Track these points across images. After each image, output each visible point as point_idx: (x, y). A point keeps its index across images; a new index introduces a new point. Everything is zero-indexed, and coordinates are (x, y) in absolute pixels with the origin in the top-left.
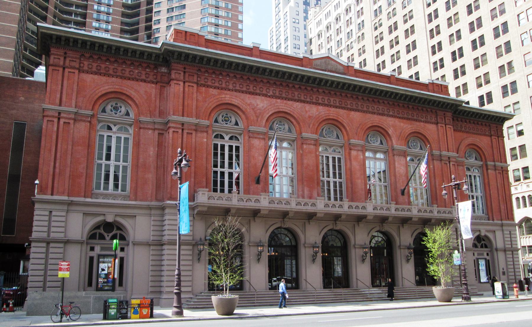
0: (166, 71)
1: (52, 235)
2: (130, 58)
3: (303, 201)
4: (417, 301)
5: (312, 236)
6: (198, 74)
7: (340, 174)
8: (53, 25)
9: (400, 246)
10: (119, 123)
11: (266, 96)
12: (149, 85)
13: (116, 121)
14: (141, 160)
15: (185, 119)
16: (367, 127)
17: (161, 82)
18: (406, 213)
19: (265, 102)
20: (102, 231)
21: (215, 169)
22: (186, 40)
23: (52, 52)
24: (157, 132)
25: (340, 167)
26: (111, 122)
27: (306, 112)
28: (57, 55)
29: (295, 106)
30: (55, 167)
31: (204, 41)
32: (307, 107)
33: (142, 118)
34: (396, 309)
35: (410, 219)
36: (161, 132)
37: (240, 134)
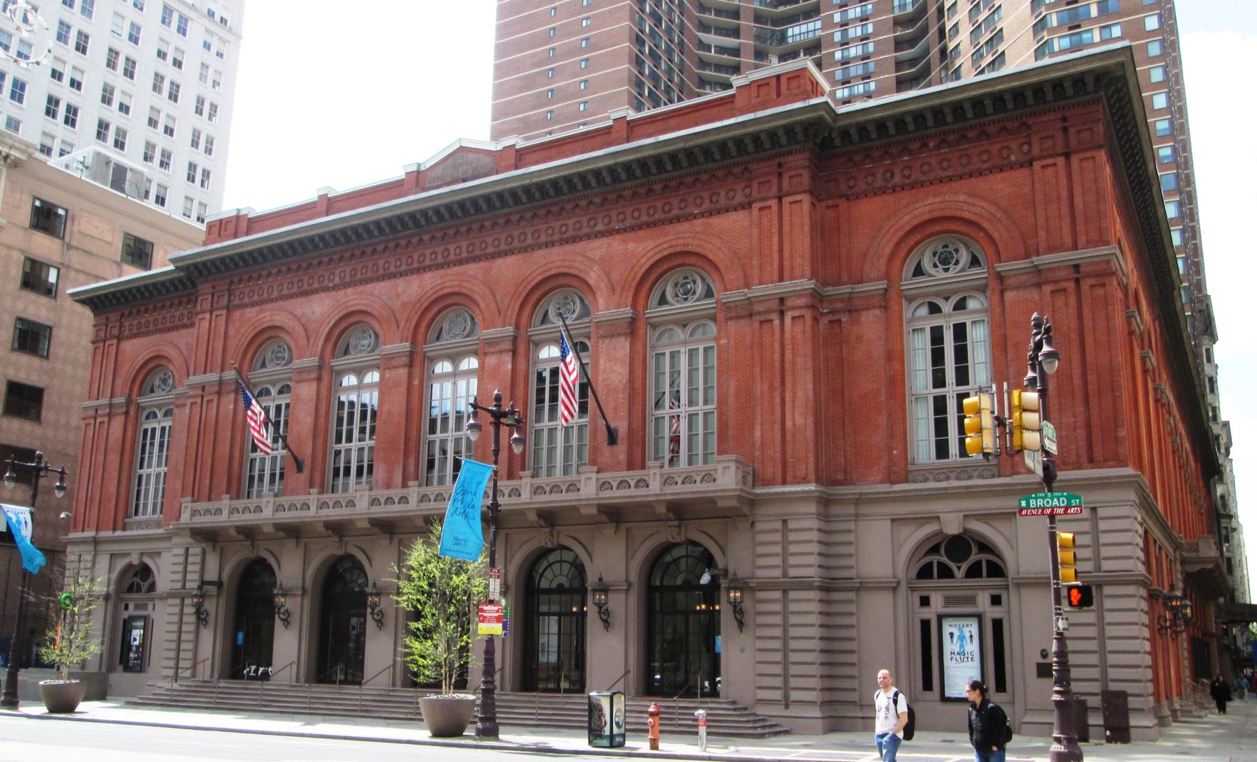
2: (973, 122)
3: (331, 499)
4: (388, 725)
5: (612, 561)
8: (898, 90)
10: (955, 292)
13: (951, 286)
20: (945, 559)
26: (936, 294)
32: (400, 283)
34: (345, 738)
35: (350, 522)
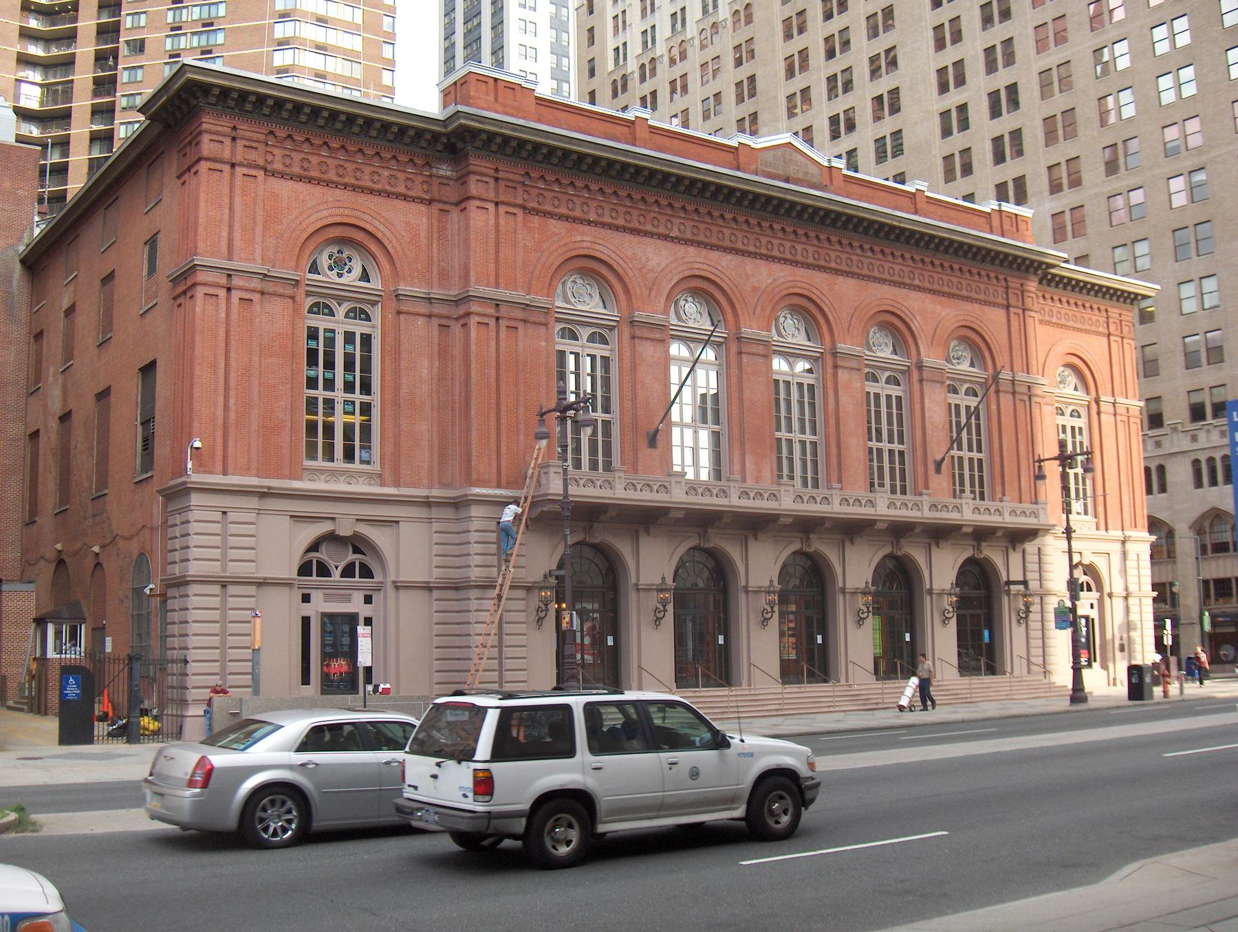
0: (448, 173)
7: (813, 423)
9: (637, 585)
11: (666, 237)
12: (415, 207)
14: (404, 391)
15: (504, 293)
16: (869, 315)
17: (440, 201)
19: (664, 253)
21: (312, 393)
22: (496, 100)
23: (204, 126)
24: (435, 322)
27: (748, 277)
29: (724, 264)
30: (226, 407)
31: (534, 102)
32: (749, 265)
33: (404, 288)
35: (957, 528)
36: (444, 322)
37: (374, 304)
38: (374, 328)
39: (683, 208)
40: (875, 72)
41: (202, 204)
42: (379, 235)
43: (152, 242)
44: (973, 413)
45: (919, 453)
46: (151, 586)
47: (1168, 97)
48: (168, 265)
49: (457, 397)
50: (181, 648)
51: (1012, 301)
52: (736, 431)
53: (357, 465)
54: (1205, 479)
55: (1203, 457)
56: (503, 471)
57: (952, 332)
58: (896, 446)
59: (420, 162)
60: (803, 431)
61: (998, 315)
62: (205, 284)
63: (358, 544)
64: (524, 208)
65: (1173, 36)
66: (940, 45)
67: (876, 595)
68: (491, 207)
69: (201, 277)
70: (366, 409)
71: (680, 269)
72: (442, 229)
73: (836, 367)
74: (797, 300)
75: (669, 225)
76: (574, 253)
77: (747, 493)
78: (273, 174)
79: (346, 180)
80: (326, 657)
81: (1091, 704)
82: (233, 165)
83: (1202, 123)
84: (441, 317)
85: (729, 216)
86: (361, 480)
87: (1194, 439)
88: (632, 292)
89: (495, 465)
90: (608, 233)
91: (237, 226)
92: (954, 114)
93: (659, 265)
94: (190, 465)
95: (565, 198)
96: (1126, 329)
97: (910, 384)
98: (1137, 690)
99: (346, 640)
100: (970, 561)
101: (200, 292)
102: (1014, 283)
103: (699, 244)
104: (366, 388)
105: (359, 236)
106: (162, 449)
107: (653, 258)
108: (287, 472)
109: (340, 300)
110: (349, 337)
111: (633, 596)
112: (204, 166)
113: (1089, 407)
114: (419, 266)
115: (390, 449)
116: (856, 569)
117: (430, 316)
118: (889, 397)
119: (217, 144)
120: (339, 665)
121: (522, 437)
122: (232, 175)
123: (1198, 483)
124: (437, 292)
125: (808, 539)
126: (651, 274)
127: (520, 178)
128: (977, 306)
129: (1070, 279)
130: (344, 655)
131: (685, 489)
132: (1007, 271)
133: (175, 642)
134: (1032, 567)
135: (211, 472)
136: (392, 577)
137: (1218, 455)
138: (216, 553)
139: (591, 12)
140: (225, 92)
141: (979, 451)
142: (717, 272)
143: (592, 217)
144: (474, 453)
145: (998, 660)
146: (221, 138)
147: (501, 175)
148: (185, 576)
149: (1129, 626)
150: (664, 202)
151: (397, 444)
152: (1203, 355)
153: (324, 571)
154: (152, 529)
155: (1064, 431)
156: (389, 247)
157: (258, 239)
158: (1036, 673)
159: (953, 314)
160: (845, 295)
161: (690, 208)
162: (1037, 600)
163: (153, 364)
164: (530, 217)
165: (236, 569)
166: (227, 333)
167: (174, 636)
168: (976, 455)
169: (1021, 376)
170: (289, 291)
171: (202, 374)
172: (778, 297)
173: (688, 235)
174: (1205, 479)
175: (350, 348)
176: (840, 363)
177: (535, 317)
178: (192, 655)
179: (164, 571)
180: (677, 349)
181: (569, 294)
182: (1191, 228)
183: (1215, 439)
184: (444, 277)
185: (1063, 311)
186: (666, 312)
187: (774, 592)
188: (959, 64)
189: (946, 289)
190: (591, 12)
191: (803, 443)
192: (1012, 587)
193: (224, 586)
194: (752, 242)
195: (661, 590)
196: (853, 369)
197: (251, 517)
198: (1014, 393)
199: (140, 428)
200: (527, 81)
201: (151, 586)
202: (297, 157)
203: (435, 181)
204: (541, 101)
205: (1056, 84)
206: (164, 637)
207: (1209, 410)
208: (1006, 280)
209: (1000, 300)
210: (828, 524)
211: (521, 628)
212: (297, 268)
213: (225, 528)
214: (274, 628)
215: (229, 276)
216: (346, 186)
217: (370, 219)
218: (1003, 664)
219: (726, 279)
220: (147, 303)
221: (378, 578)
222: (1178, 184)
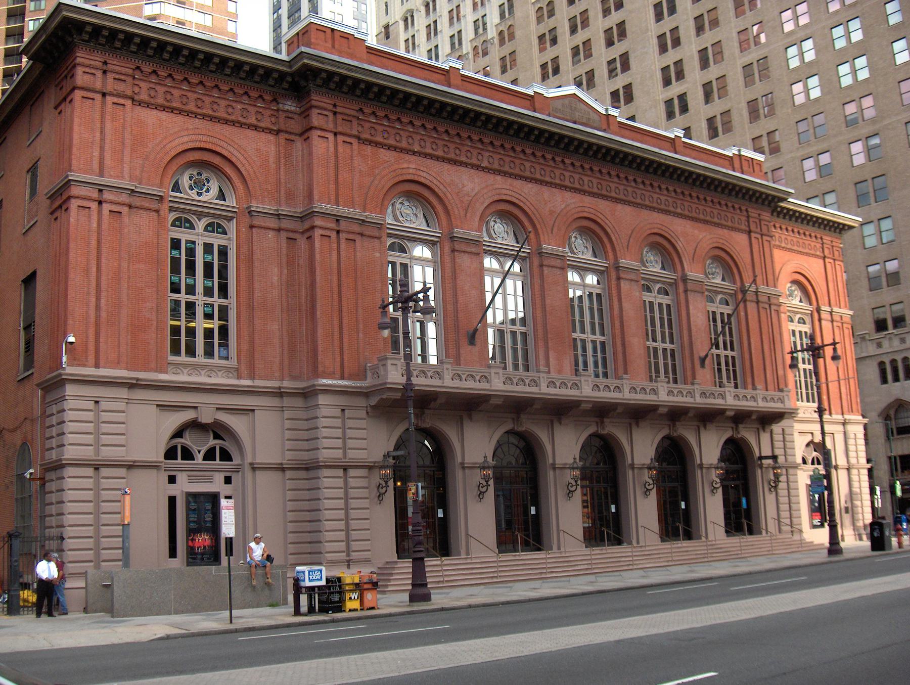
0: (293, 108)
1: (351, 454)
6: (358, 118)
7: (602, 326)
9: (462, 463)
11: (478, 167)
12: (263, 136)
14: (257, 294)
15: (343, 210)
17: (286, 132)
18: (648, 397)
19: (476, 180)
21: (176, 296)
22: (333, 47)
23: (79, 60)
24: (284, 235)
25: (600, 311)
28: (90, 66)
30: (98, 308)
31: (365, 50)
33: (255, 206)
36: (291, 235)
37: (229, 219)
38: (230, 240)
39: (491, 143)
40: (612, 73)
41: (76, 128)
42: (234, 159)
43: (33, 170)
44: (727, 321)
45: (687, 353)
46: (31, 471)
47: (846, 81)
48: (45, 186)
49: (303, 301)
50: (58, 527)
51: (753, 227)
52: (540, 332)
53: (216, 361)
54: (890, 377)
55: (887, 360)
56: (346, 364)
57: (708, 252)
58: (668, 346)
59: (268, 98)
60: (594, 333)
61: (742, 238)
62: (77, 197)
63: (218, 430)
64: (359, 138)
65: (848, 34)
66: (663, 49)
67: (660, 471)
68: (331, 136)
69: (75, 191)
70: (223, 311)
71: (490, 194)
72: (288, 156)
73: (619, 278)
74: (586, 223)
75: (480, 157)
76: (401, 178)
77: (553, 383)
78: (140, 103)
79: (204, 111)
80: (191, 532)
81: (846, 555)
82: (104, 95)
83: (874, 99)
84: (287, 230)
85: (529, 151)
86: (220, 373)
87: (879, 345)
88: (451, 212)
89: (338, 359)
90: (430, 162)
91: (107, 147)
92: (676, 102)
93: (473, 190)
94: (64, 359)
95: (393, 131)
96: (836, 253)
97: (677, 294)
98: (878, 543)
99: (209, 517)
100: (730, 442)
101: (74, 204)
102: (753, 213)
103: (505, 174)
104: (224, 291)
105: (216, 160)
106: (41, 349)
107: (468, 184)
108: (153, 365)
109: (200, 215)
110: (208, 248)
111: (459, 474)
112: (78, 94)
113: (812, 315)
114: (269, 187)
115: (245, 346)
116: (641, 448)
117: (279, 230)
118: (660, 305)
119: (89, 76)
120: (203, 540)
121: (361, 335)
122: (103, 103)
123: (884, 380)
124: (285, 210)
125: (602, 422)
126: (466, 198)
127: (355, 113)
128: (726, 231)
129: (795, 212)
130: (207, 530)
131: (503, 379)
132: (747, 203)
133: (52, 521)
134: (779, 444)
135: (85, 366)
136: (249, 459)
137: (899, 358)
138: (89, 439)
139: (388, 37)
140: (97, 30)
141: (732, 349)
142: (521, 198)
143: (416, 148)
144: (320, 349)
145: (624, 535)
146: (93, 71)
147: (339, 109)
148: (61, 460)
149: (851, 495)
150: (475, 138)
151: (252, 342)
152: (884, 280)
153: (188, 455)
154: (32, 420)
155: (794, 335)
156: (242, 169)
157: (127, 159)
158: (786, 532)
159: (708, 237)
160: (624, 219)
161: (497, 143)
162: (784, 471)
163: (33, 275)
164: (364, 147)
165: (107, 453)
166: (99, 242)
167: (51, 515)
168: (729, 353)
169: (763, 288)
170: (154, 206)
171: (75, 278)
172: (571, 220)
173: (496, 166)
174: (890, 377)
175: (208, 258)
176: (622, 275)
177: (370, 231)
178: (69, 531)
179: (43, 458)
180: (489, 262)
181: (398, 213)
182: (870, 181)
183: (896, 343)
184: (290, 196)
185: (789, 238)
186: (480, 230)
187: (577, 468)
188: (679, 63)
189: (701, 216)
190: (388, 37)
191: (594, 342)
192: (764, 461)
193: (97, 469)
194: (548, 173)
195: (483, 468)
196: (632, 280)
197: (121, 406)
198: (758, 302)
199: (22, 333)
200: (359, 32)
201: (31, 471)
202: (161, 90)
203: (282, 115)
204: (371, 50)
205: (757, 75)
206: (43, 517)
207: (890, 323)
208: (747, 211)
209: (743, 227)
210: (620, 410)
211: (365, 503)
212: (161, 185)
213: (97, 416)
214: (142, 507)
215: (100, 191)
216: (204, 116)
217: (225, 145)
218: (698, 530)
219: (528, 203)
220: (28, 223)
221: (236, 460)
222: (857, 147)
